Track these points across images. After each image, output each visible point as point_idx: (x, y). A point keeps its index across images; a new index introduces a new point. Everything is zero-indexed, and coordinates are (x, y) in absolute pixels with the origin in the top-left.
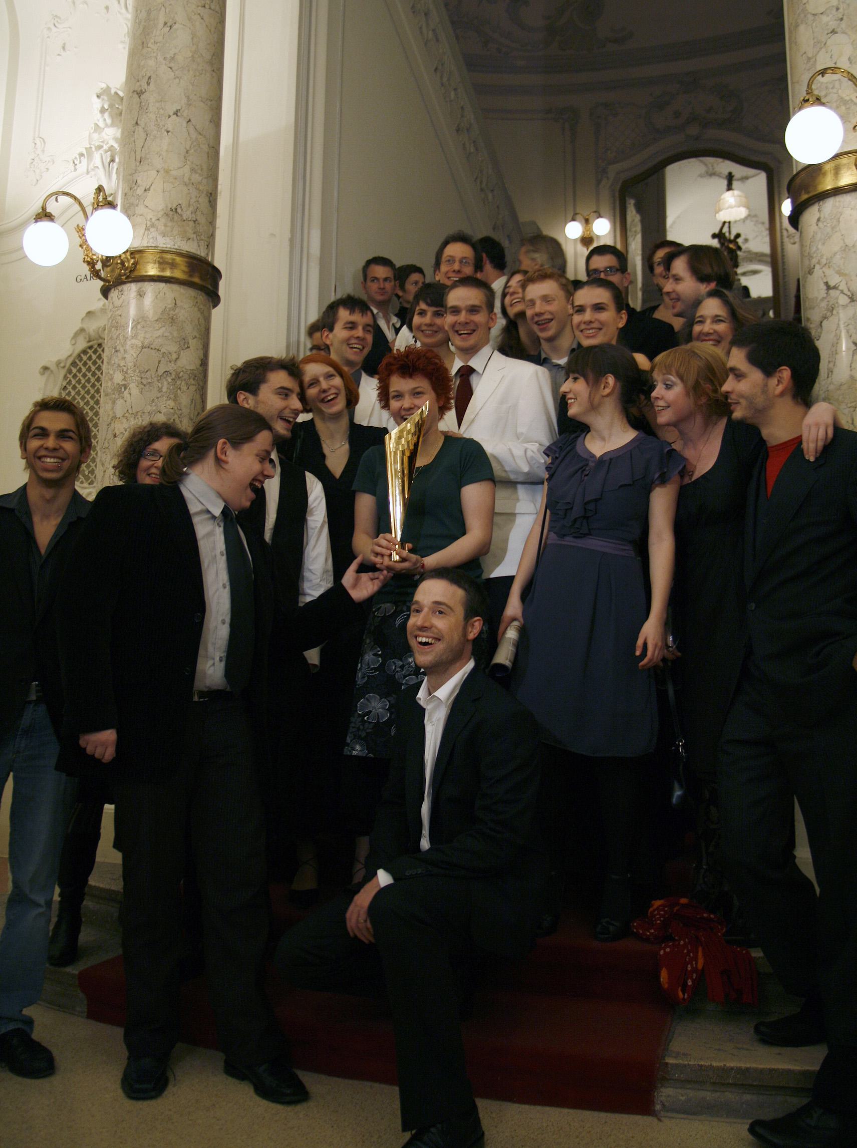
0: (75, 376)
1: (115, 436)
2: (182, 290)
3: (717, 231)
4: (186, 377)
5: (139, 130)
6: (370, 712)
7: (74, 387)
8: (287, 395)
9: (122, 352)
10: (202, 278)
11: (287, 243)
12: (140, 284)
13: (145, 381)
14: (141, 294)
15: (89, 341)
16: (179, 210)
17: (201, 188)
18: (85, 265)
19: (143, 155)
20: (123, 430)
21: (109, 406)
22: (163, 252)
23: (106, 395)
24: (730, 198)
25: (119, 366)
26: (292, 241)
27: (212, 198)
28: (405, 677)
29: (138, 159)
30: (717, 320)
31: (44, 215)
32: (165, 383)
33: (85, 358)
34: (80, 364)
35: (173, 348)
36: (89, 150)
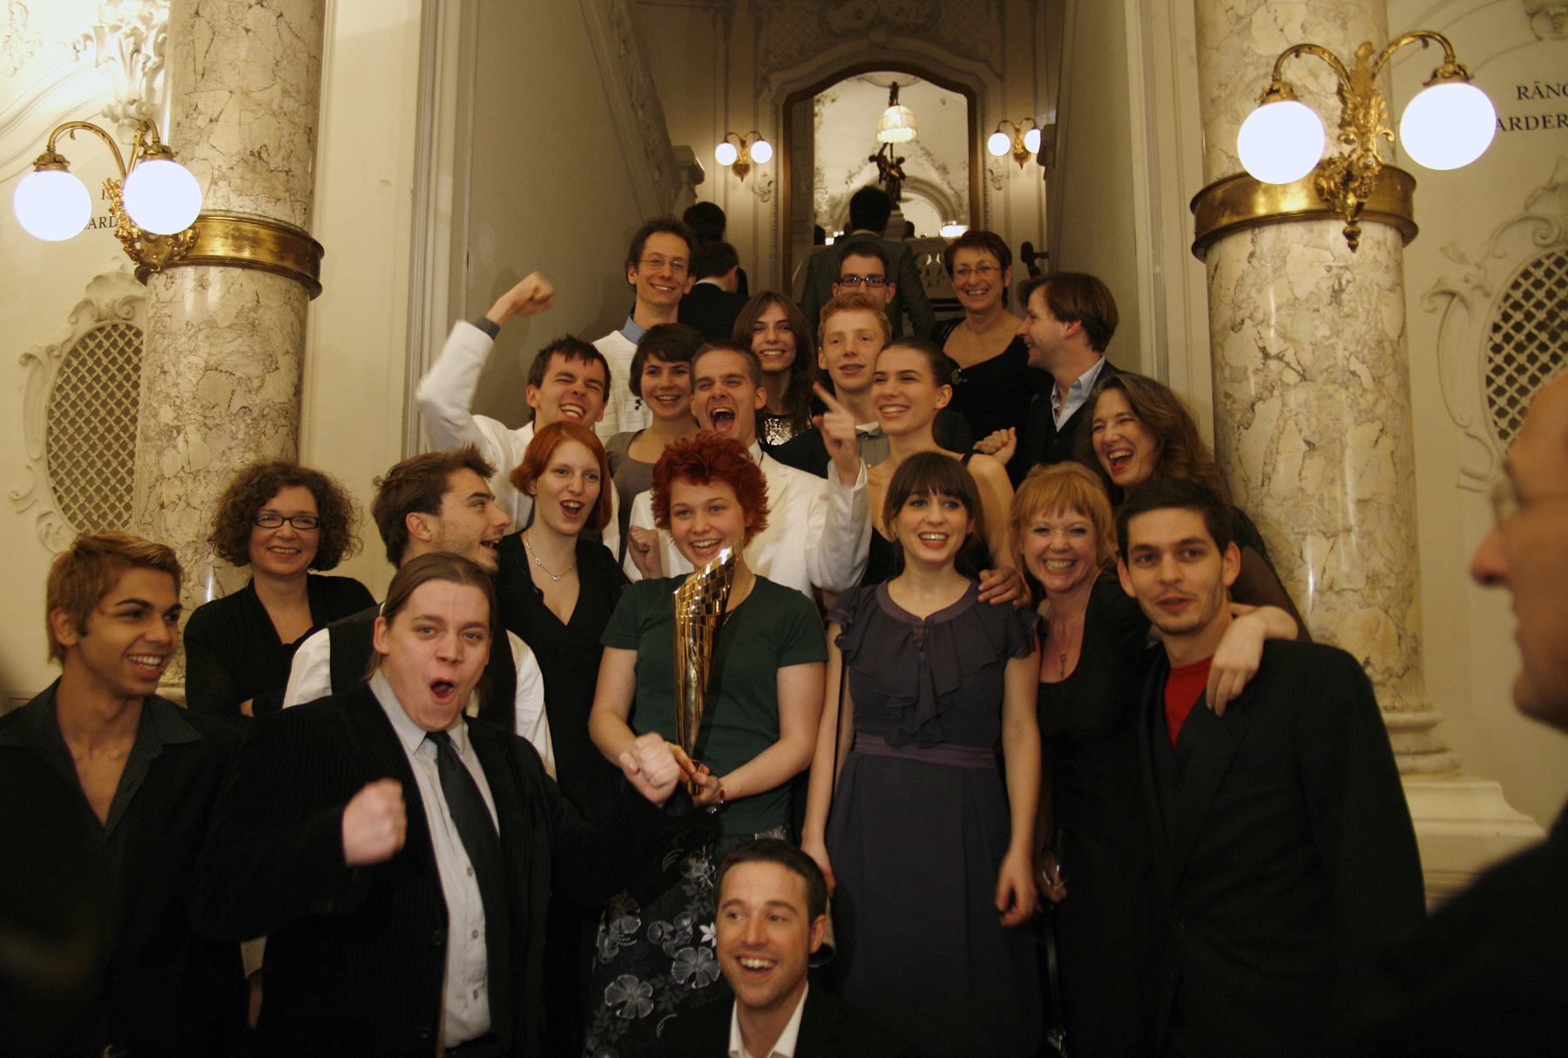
0: (76, 371)
1: (162, 506)
2: (268, 280)
3: (876, 152)
4: (274, 414)
5: (201, 24)
6: (625, 1003)
7: (75, 388)
8: (482, 503)
9: (173, 372)
10: (296, 258)
11: (408, 198)
12: (201, 269)
13: (210, 423)
14: (202, 285)
15: (99, 320)
16: (264, 155)
17: (297, 120)
18: (119, 241)
19: (208, 65)
20: (175, 499)
21: (151, 458)
22: (240, 220)
23: (147, 439)
24: (895, 115)
25: (168, 395)
26: (414, 192)
27: (311, 134)
28: (677, 949)
29: (200, 69)
30: (1120, 420)
31: (52, 160)
32: (242, 426)
33: (92, 345)
34: (85, 354)
35: (255, 370)
36: (99, 30)
